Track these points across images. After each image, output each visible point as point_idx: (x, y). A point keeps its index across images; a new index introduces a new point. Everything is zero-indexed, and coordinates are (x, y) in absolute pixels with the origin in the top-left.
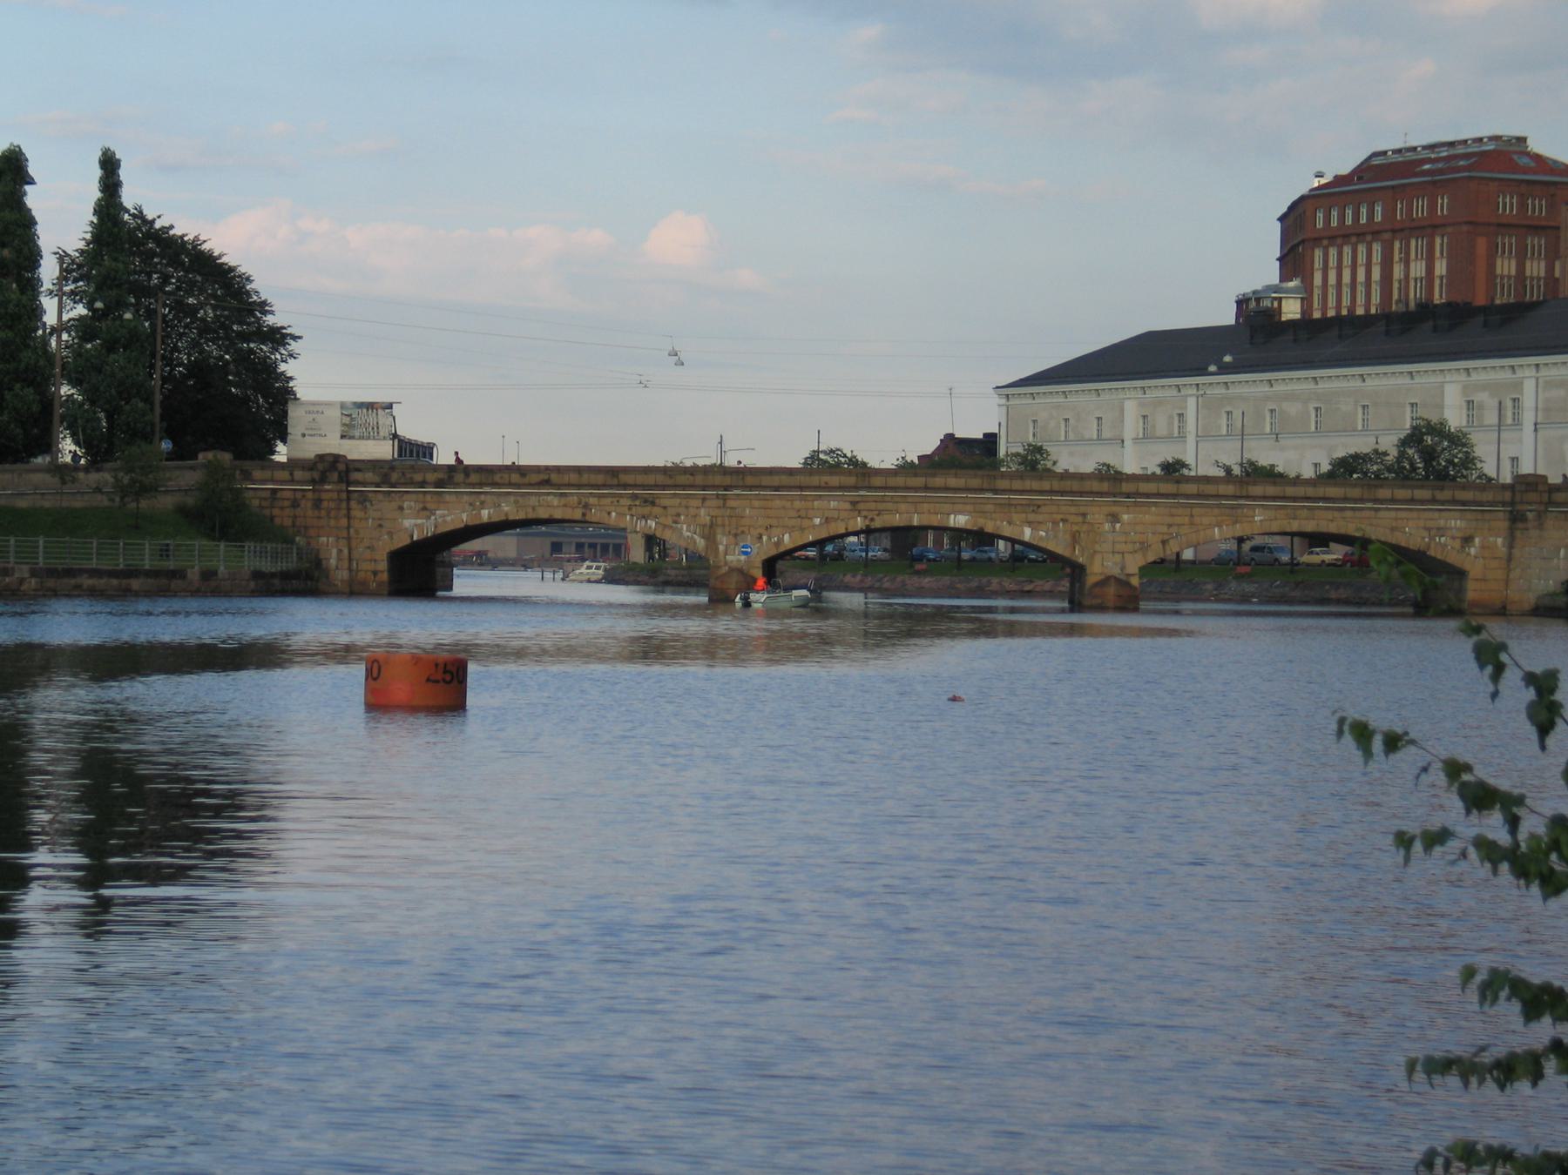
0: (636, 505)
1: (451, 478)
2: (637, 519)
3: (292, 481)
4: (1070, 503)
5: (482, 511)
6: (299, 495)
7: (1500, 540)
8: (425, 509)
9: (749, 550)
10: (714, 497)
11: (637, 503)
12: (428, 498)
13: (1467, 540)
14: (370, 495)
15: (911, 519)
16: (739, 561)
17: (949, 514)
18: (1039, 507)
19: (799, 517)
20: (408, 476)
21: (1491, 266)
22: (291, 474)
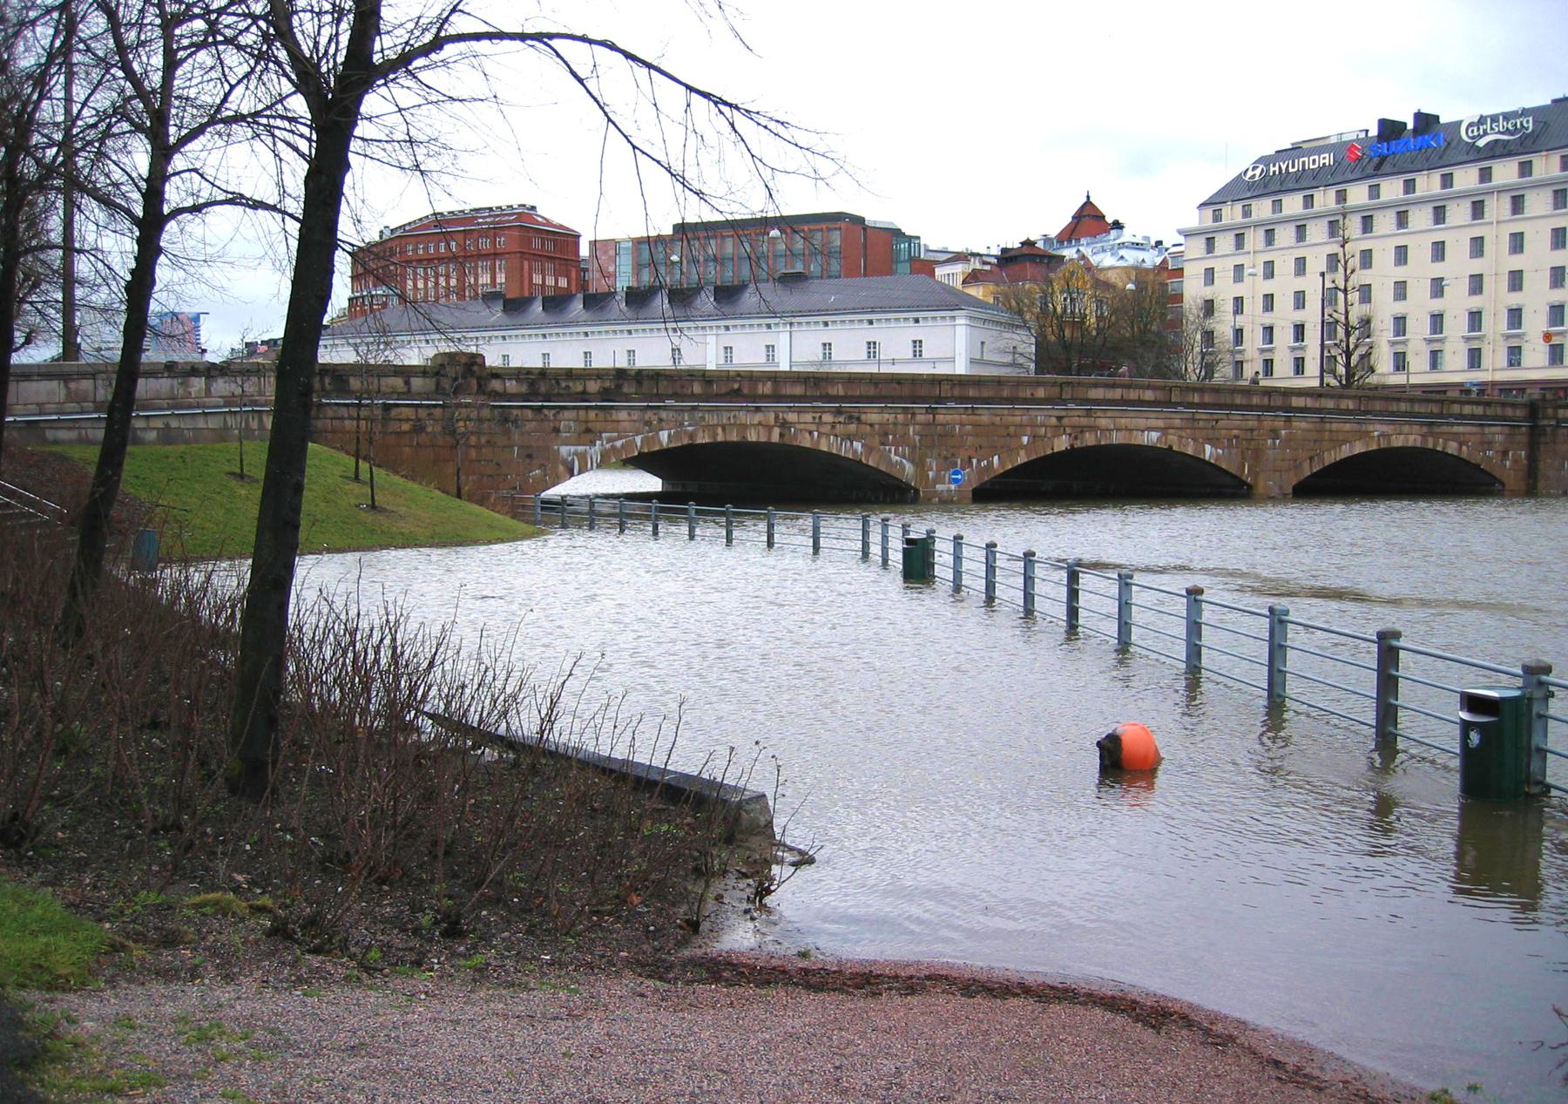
0: (840, 422)
1: (619, 387)
2: (842, 440)
3: (408, 394)
4: (1318, 420)
5: (661, 433)
6: (423, 413)
7: (1523, 453)
8: (588, 431)
9: (959, 477)
10: (924, 411)
11: (841, 419)
12: (592, 414)
13: (1505, 453)
14: (515, 412)
15: (657, 439)
16: (949, 491)
17: (1143, 431)
18: (1217, 421)
19: (1008, 435)
20: (563, 384)
21: (531, 279)
22: (407, 383)
